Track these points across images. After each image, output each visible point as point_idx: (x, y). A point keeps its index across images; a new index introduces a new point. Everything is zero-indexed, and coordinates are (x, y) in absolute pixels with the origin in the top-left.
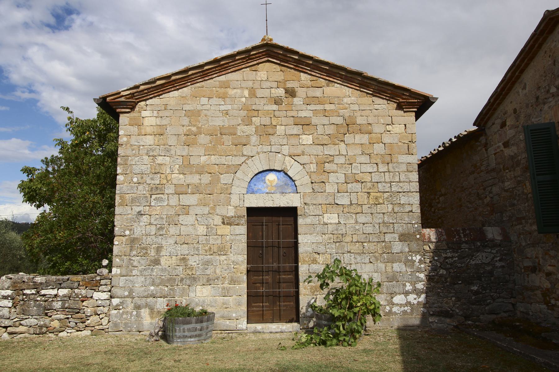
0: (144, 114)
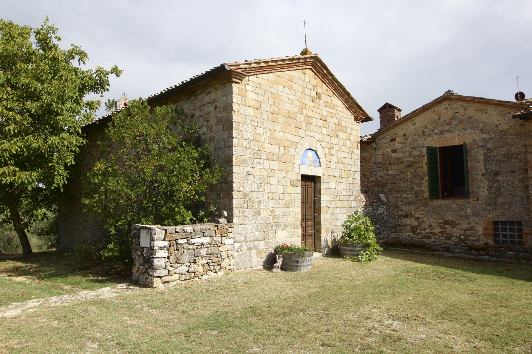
0: (249, 88)
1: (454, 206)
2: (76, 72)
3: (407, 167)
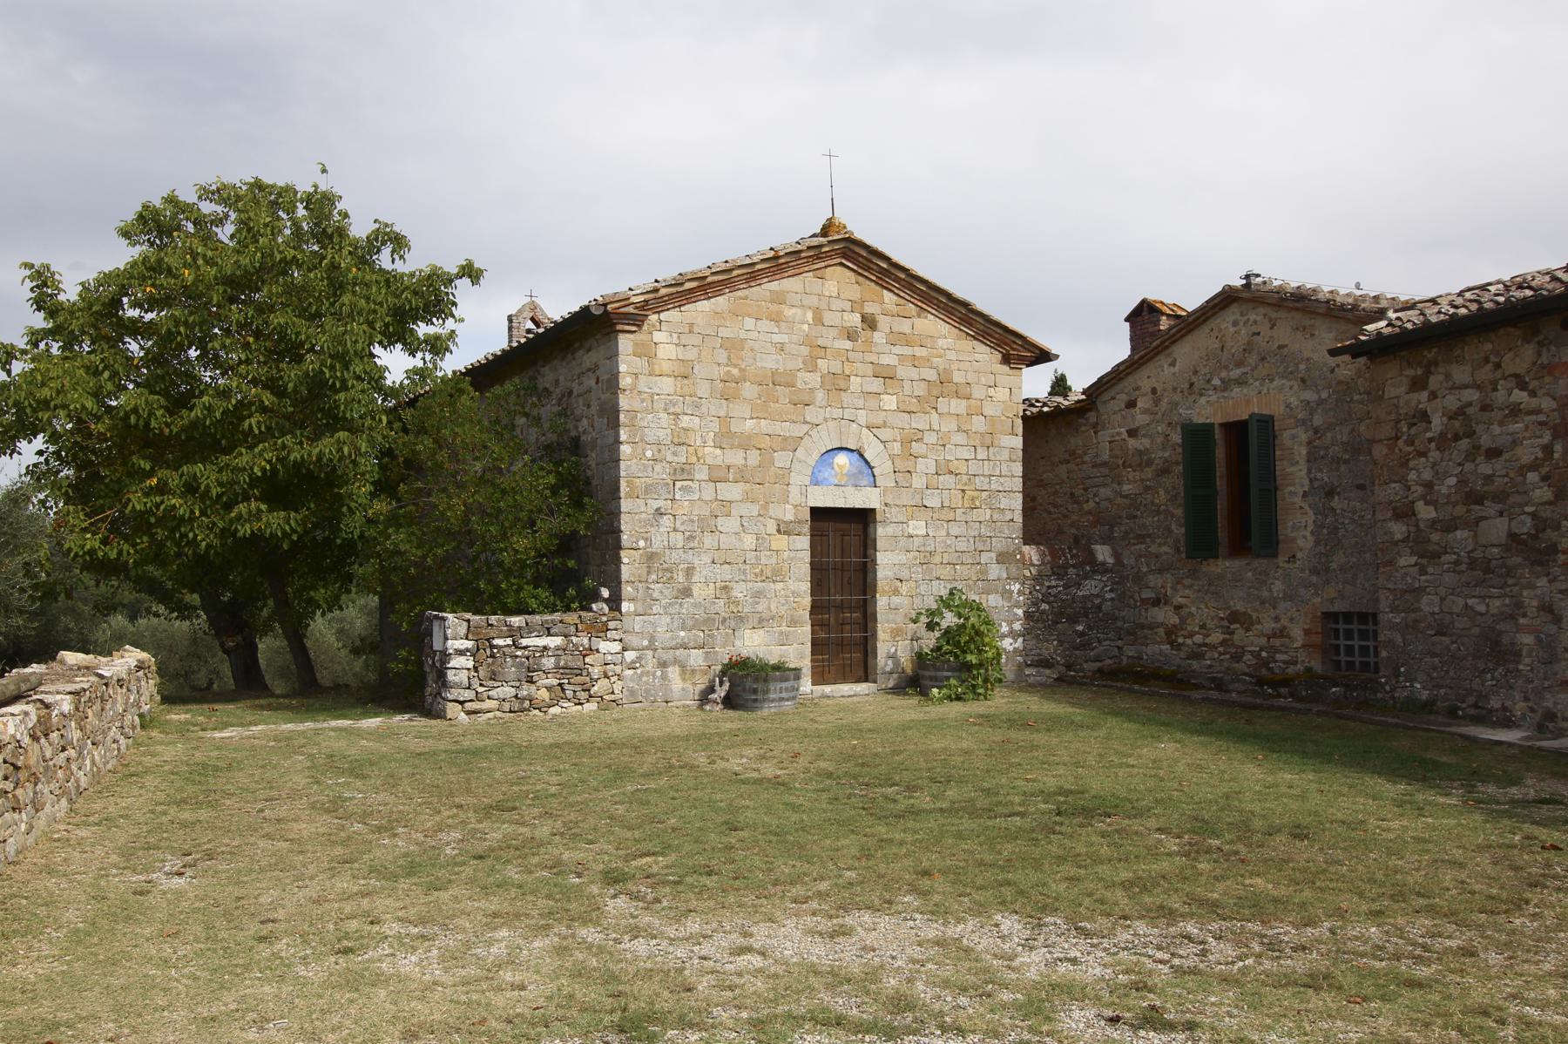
0: (658, 336)
2: (389, 279)
3: (1158, 475)
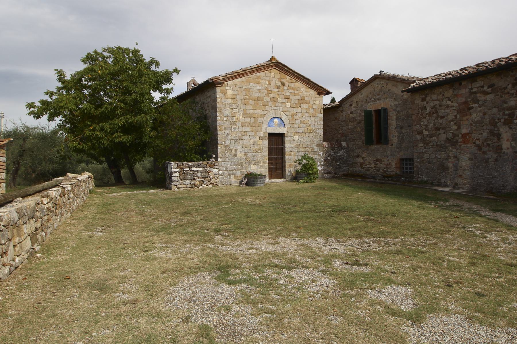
0: (227, 88)
1: (381, 149)
